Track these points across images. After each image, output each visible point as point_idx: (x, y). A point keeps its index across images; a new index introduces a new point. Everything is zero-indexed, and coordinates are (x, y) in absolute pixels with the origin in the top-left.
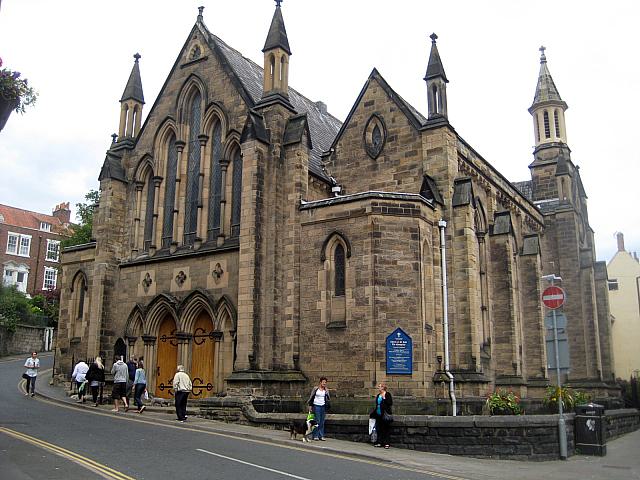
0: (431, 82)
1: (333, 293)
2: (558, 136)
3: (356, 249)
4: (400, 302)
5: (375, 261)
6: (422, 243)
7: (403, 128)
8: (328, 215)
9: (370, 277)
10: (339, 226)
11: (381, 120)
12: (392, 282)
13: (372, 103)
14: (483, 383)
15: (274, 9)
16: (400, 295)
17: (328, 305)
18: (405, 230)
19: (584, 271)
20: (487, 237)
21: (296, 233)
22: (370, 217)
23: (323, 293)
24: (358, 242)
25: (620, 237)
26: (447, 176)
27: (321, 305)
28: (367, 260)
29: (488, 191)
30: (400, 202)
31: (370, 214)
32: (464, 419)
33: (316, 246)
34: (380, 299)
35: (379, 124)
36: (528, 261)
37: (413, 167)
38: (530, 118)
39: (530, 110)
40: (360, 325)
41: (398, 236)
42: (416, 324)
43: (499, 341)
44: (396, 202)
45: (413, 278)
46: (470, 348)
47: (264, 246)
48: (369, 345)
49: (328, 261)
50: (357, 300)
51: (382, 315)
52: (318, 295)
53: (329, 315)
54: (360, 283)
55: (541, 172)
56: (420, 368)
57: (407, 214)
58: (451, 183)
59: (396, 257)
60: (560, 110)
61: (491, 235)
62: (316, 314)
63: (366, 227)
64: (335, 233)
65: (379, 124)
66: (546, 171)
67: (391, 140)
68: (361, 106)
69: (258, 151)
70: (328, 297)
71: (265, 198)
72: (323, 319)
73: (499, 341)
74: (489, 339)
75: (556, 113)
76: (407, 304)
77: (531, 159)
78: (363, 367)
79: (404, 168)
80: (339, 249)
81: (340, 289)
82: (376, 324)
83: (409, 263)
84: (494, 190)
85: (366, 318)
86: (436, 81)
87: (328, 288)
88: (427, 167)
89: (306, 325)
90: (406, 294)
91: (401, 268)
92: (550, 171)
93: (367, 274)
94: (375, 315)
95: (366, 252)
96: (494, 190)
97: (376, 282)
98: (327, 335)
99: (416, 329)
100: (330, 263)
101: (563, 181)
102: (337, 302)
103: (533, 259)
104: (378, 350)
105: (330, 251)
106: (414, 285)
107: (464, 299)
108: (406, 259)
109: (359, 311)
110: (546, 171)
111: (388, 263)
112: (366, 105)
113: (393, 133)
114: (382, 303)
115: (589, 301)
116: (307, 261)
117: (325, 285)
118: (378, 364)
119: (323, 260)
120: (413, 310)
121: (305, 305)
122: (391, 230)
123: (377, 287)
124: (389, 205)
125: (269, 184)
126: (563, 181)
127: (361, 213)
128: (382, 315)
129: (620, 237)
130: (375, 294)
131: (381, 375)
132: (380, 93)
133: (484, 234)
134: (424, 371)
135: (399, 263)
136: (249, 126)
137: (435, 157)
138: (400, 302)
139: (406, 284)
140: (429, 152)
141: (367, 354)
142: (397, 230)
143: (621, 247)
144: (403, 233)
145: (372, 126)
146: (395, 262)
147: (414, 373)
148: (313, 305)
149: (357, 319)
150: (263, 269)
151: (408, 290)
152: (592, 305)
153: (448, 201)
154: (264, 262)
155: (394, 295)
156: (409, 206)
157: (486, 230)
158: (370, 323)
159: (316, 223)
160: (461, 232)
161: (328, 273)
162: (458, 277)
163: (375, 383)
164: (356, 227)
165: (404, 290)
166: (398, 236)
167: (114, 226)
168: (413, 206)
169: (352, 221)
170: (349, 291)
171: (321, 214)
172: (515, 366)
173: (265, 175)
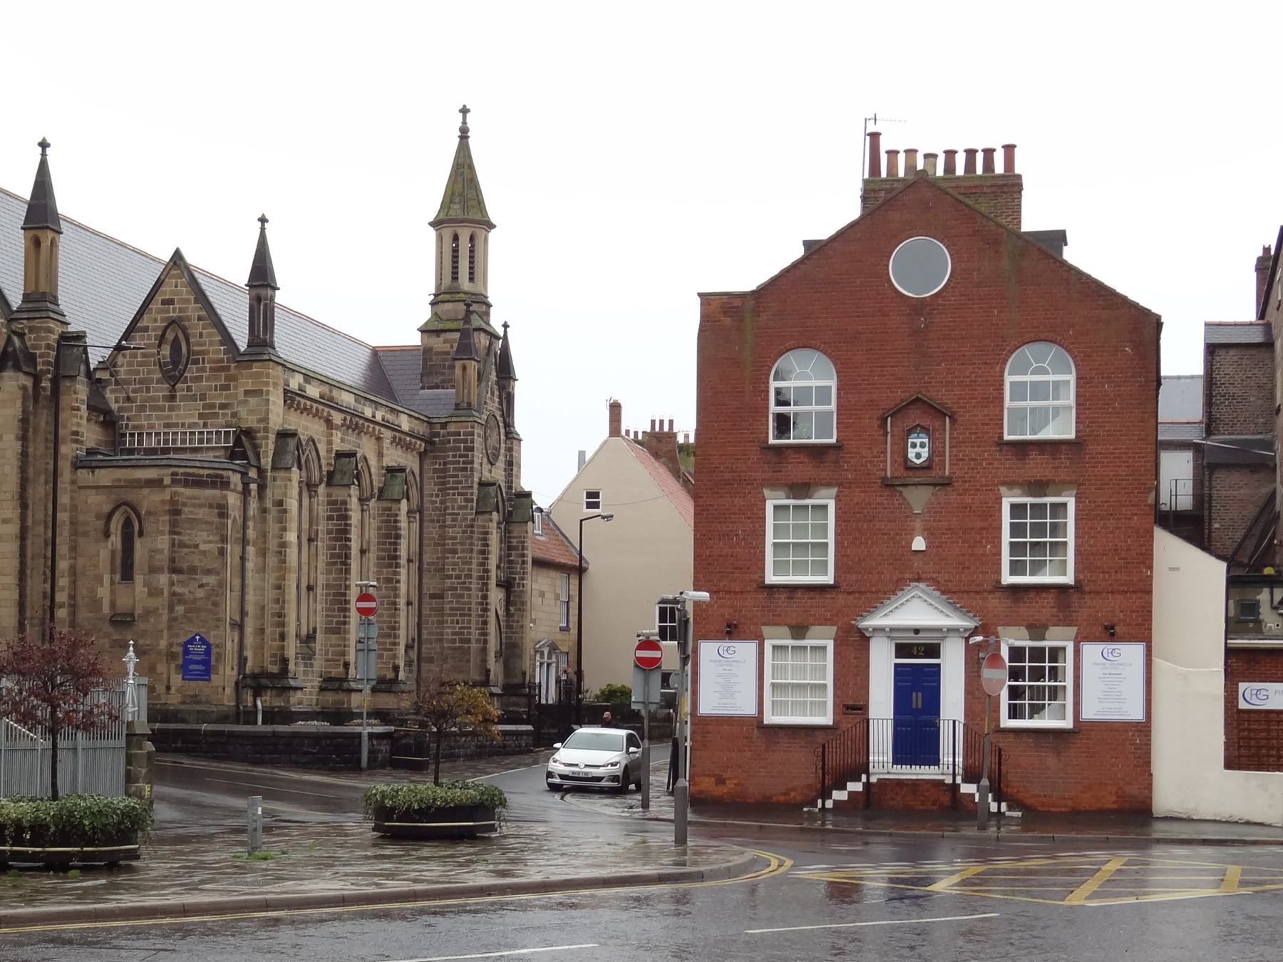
0: (255, 292)
1: (118, 577)
2: (471, 279)
3: (149, 526)
4: (201, 593)
5: (173, 545)
6: (230, 522)
7: (217, 352)
8: (113, 481)
9: (166, 564)
10: (132, 496)
11: (184, 330)
12: (193, 570)
13: (171, 302)
14: (296, 689)
15: (39, 158)
16: (201, 586)
17: (113, 592)
18: (211, 506)
19: (480, 517)
20: (322, 489)
21: (72, 498)
22: (168, 491)
23: (107, 578)
24: (152, 519)
25: (615, 409)
26: (266, 430)
27: (104, 592)
28: (163, 542)
29: (329, 422)
30: (207, 472)
31: (169, 486)
32: (269, 728)
33: (98, 517)
34: (178, 589)
35: (181, 336)
36: (389, 509)
37: (223, 406)
38: (432, 233)
39: (433, 224)
40: (152, 620)
41: (202, 513)
42: (218, 620)
43: (329, 631)
44: (201, 472)
45: (216, 565)
46: (282, 648)
47: (30, 513)
48: (163, 644)
49: (113, 537)
50: (149, 590)
51: (180, 609)
52: (99, 580)
53: (113, 604)
54: (153, 570)
55: (438, 343)
56: (221, 672)
57: (214, 485)
58: (272, 437)
59: (198, 540)
60: (480, 233)
61: (329, 484)
62: (96, 603)
63: (163, 502)
64: (125, 503)
65: (181, 336)
66: (445, 342)
67: (196, 362)
68: (156, 305)
69: (24, 388)
70: (112, 583)
71: (31, 450)
72: (106, 609)
73: (329, 631)
74: (315, 630)
75: (472, 239)
76: (208, 597)
77: (425, 314)
78: (155, 670)
79: (212, 406)
80: (127, 524)
81: (127, 571)
82: (172, 620)
83: (213, 547)
84: (337, 418)
85: (160, 611)
86: (262, 292)
87: (113, 572)
88: (243, 412)
89: (83, 615)
90: (208, 584)
91: (203, 553)
92: (451, 342)
93: (163, 559)
94: (171, 608)
95: (162, 533)
96: (337, 418)
97: (174, 570)
98: (111, 629)
99: (218, 627)
100: (116, 540)
101: (464, 368)
102: (122, 589)
103: (394, 506)
104: (174, 650)
105: (116, 525)
106: (218, 573)
107: (279, 587)
108: (210, 542)
109: (152, 603)
110: (445, 342)
111: (188, 547)
112: (165, 302)
113: (199, 353)
114: (179, 594)
115: (483, 564)
116: (85, 534)
117: (108, 567)
118: (173, 666)
119: (107, 534)
120: (215, 604)
121: (82, 591)
122: (194, 506)
123: (175, 577)
124: (189, 474)
125: (35, 431)
126: (464, 368)
127: (156, 484)
128: (180, 609)
129: (615, 409)
130: (172, 584)
131: (177, 679)
132: (185, 292)
133: (317, 486)
134: (226, 674)
135: (202, 547)
136: (10, 349)
137: (253, 401)
138: (201, 593)
139: (209, 572)
140: (247, 393)
141: (159, 653)
142: (200, 506)
143: (615, 428)
144: (206, 510)
145: (170, 336)
146: (196, 546)
147: (213, 676)
148: (93, 592)
149: (148, 613)
150: (29, 542)
151: (211, 580)
152: (487, 571)
153: (267, 462)
154: (30, 536)
155: (194, 585)
156: (217, 476)
157: (321, 481)
158: (165, 618)
159: (97, 487)
160: (280, 503)
161: (113, 553)
162: (272, 560)
163: (168, 688)
164: (150, 500)
165: (206, 579)
166: (202, 513)
167: (365, 796)
168: (222, 477)
169: (146, 491)
170: (139, 578)
171: (105, 477)
172: (346, 665)
173: (31, 418)
